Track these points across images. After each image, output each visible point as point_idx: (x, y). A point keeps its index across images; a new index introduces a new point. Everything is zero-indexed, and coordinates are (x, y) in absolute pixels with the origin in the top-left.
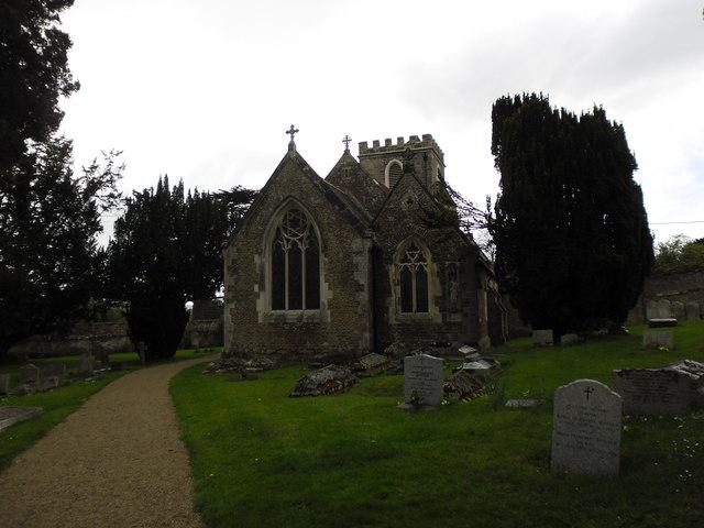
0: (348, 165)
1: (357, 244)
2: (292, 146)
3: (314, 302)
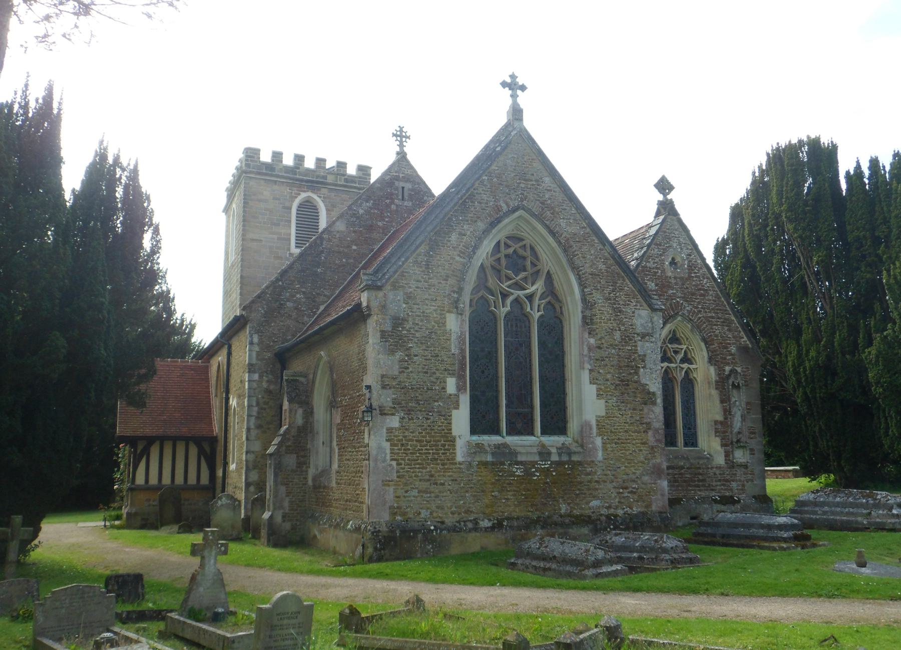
2: (516, 113)
3: (556, 422)
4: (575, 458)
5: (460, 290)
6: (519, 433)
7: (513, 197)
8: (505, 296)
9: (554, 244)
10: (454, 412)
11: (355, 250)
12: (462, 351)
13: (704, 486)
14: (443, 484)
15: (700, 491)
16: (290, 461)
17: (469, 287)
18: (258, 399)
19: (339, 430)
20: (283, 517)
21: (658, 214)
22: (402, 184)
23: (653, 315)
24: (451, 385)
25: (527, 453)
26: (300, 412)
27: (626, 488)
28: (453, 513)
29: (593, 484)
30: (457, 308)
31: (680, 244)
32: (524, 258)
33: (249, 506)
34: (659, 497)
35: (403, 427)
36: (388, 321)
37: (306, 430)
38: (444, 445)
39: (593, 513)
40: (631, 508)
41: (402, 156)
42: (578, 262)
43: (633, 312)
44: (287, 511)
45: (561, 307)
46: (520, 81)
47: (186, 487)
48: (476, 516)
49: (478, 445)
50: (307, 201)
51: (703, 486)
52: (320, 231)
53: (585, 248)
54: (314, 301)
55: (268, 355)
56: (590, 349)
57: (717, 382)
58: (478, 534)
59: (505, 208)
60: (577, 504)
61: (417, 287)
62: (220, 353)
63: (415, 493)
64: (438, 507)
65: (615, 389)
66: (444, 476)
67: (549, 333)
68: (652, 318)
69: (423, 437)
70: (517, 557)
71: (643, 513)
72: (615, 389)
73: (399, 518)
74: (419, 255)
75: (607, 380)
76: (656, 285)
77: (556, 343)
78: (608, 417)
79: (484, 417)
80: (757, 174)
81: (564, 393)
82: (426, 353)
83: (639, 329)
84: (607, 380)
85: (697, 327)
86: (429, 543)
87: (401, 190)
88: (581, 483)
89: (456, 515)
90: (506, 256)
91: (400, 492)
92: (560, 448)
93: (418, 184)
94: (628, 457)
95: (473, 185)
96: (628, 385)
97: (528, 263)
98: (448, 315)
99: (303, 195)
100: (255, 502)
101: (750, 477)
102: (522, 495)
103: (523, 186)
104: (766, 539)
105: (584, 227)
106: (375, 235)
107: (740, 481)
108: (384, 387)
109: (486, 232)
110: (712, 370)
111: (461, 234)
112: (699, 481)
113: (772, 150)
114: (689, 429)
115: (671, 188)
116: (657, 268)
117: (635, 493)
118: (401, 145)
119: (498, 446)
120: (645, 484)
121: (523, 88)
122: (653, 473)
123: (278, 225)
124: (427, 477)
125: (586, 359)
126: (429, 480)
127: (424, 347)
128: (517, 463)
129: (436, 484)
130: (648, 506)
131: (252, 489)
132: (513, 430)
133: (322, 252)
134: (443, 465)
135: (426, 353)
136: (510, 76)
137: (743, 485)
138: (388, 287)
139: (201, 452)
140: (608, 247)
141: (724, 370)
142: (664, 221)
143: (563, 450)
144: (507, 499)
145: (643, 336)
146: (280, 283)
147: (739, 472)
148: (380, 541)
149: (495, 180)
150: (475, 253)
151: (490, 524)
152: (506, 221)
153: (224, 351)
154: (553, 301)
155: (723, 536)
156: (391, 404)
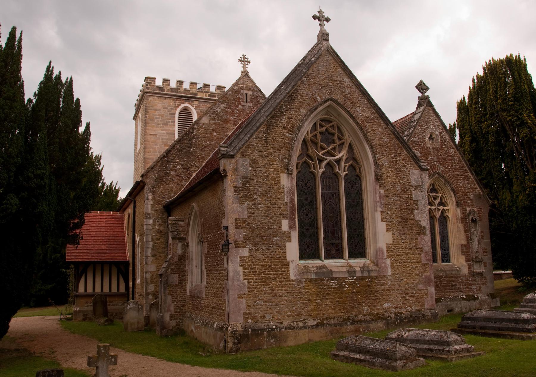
0: (249, 89)
1: (414, 175)
2: (324, 36)
3: (358, 249)
4: (373, 274)
5: (290, 157)
6: (333, 258)
7: (325, 92)
8: (321, 161)
9: (354, 124)
10: (288, 244)
11: (215, 136)
12: (293, 200)
14: (281, 296)
16: (175, 278)
17: (296, 154)
18: (152, 236)
19: (206, 257)
20: (171, 317)
21: (419, 105)
22: (245, 92)
23: (422, 173)
24: (285, 224)
25: (340, 272)
26: (180, 245)
27: (407, 294)
28: (288, 316)
29: (386, 292)
30: (288, 170)
32: (333, 134)
33: (148, 308)
34: (430, 298)
36: (239, 180)
37: (184, 258)
38: (281, 268)
39: (385, 312)
41: (245, 74)
42: (370, 136)
43: (409, 171)
44: (173, 313)
45: (360, 169)
46: (326, 15)
47: (111, 295)
49: (305, 267)
50: (185, 109)
51: (455, 289)
52: (193, 121)
53: (374, 128)
54: (189, 170)
55: (159, 207)
56: (380, 197)
57: (462, 218)
58: (307, 330)
60: (375, 306)
62: (130, 206)
66: (282, 290)
67: (352, 187)
69: (265, 262)
70: (338, 350)
74: (260, 133)
75: (393, 219)
76: (421, 153)
77: (357, 193)
78: (394, 244)
79: (308, 247)
80: (476, 81)
81: (363, 228)
83: (413, 183)
84: (393, 219)
86: (272, 338)
87: (245, 95)
89: (291, 317)
90: (321, 133)
91: (251, 303)
92: (362, 268)
94: (409, 272)
95: (296, 84)
97: (336, 138)
98: (281, 175)
99: (183, 106)
100: (152, 306)
103: (331, 84)
104: (508, 329)
105: (373, 113)
106: (228, 126)
107: (478, 284)
109: (307, 116)
110: (459, 210)
111: (289, 118)
112: (453, 285)
113: (486, 65)
114: (445, 250)
115: (427, 89)
116: (421, 142)
118: (244, 67)
119: (319, 268)
121: (328, 20)
123: (167, 125)
124: (270, 291)
125: (378, 204)
126: (271, 293)
127: (265, 198)
128: (333, 279)
129: (276, 296)
131: (150, 297)
132: (328, 256)
133: (193, 137)
136: (319, 12)
137: (480, 287)
138: (239, 155)
139: (119, 272)
140: (390, 126)
141: (466, 210)
142: (424, 110)
143: (364, 268)
145: (416, 187)
146: (166, 159)
147: (478, 278)
148: (237, 338)
149: (312, 80)
150: (299, 131)
151: (315, 323)
152: (321, 108)
153: (132, 206)
154: (355, 164)
155: (481, 328)
156: (242, 239)
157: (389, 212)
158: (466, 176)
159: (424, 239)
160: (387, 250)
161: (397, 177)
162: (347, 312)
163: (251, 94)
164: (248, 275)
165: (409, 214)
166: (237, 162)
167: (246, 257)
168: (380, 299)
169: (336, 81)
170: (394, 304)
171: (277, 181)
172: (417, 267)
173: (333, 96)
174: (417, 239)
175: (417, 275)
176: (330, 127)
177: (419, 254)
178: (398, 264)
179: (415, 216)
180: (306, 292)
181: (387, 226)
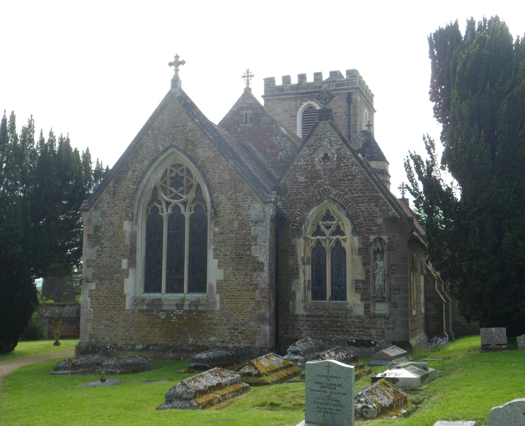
2: (176, 82)
3: (199, 283)
4: (200, 308)
13: (342, 331)
14: (117, 322)
15: (338, 334)
27: (237, 329)
28: (123, 339)
31: (330, 142)
34: (262, 336)
35: (98, 289)
36: (92, 229)
38: (119, 300)
39: (211, 345)
40: (239, 344)
42: (209, 176)
43: (249, 206)
48: (136, 342)
57: (360, 249)
59: (161, 148)
61: (108, 207)
63: (102, 326)
64: (114, 335)
65: (232, 261)
68: (264, 209)
71: (248, 348)
72: (232, 261)
73: (93, 340)
75: (226, 255)
76: (306, 178)
82: (111, 246)
83: (253, 217)
84: (226, 255)
85: (342, 206)
88: (203, 325)
89: (124, 341)
93: (257, 109)
96: (242, 258)
97: (185, 182)
98: (124, 222)
99: (305, 104)
101: (391, 326)
102: (164, 331)
105: (215, 151)
108: (88, 266)
111: (134, 171)
112: (337, 327)
117: (243, 333)
118: (248, 83)
120: (252, 327)
122: (258, 320)
124: (110, 318)
126: (110, 320)
127: (110, 242)
130: (253, 343)
134: (119, 311)
135: (111, 246)
137: (383, 332)
138: (92, 209)
141: (369, 239)
143: (197, 303)
144: (155, 333)
145: (256, 222)
149: (156, 131)
154: (200, 204)
156: (91, 276)
157: (222, 249)
158: (373, 197)
159: (260, 276)
160: (217, 286)
161: (235, 213)
162: (173, 340)
163: (251, 112)
164: (94, 304)
165: (245, 250)
166: (90, 214)
167: (94, 290)
168: (206, 332)
169: (180, 127)
170: (221, 338)
171: (121, 227)
172: (248, 304)
173: (174, 143)
174: (252, 275)
175: (250, 312)
176: (171, 173)
177: (254, 290)
178: (229, 300)
179: (253, 252)
180: (138, 321)
181: (219, 263)
